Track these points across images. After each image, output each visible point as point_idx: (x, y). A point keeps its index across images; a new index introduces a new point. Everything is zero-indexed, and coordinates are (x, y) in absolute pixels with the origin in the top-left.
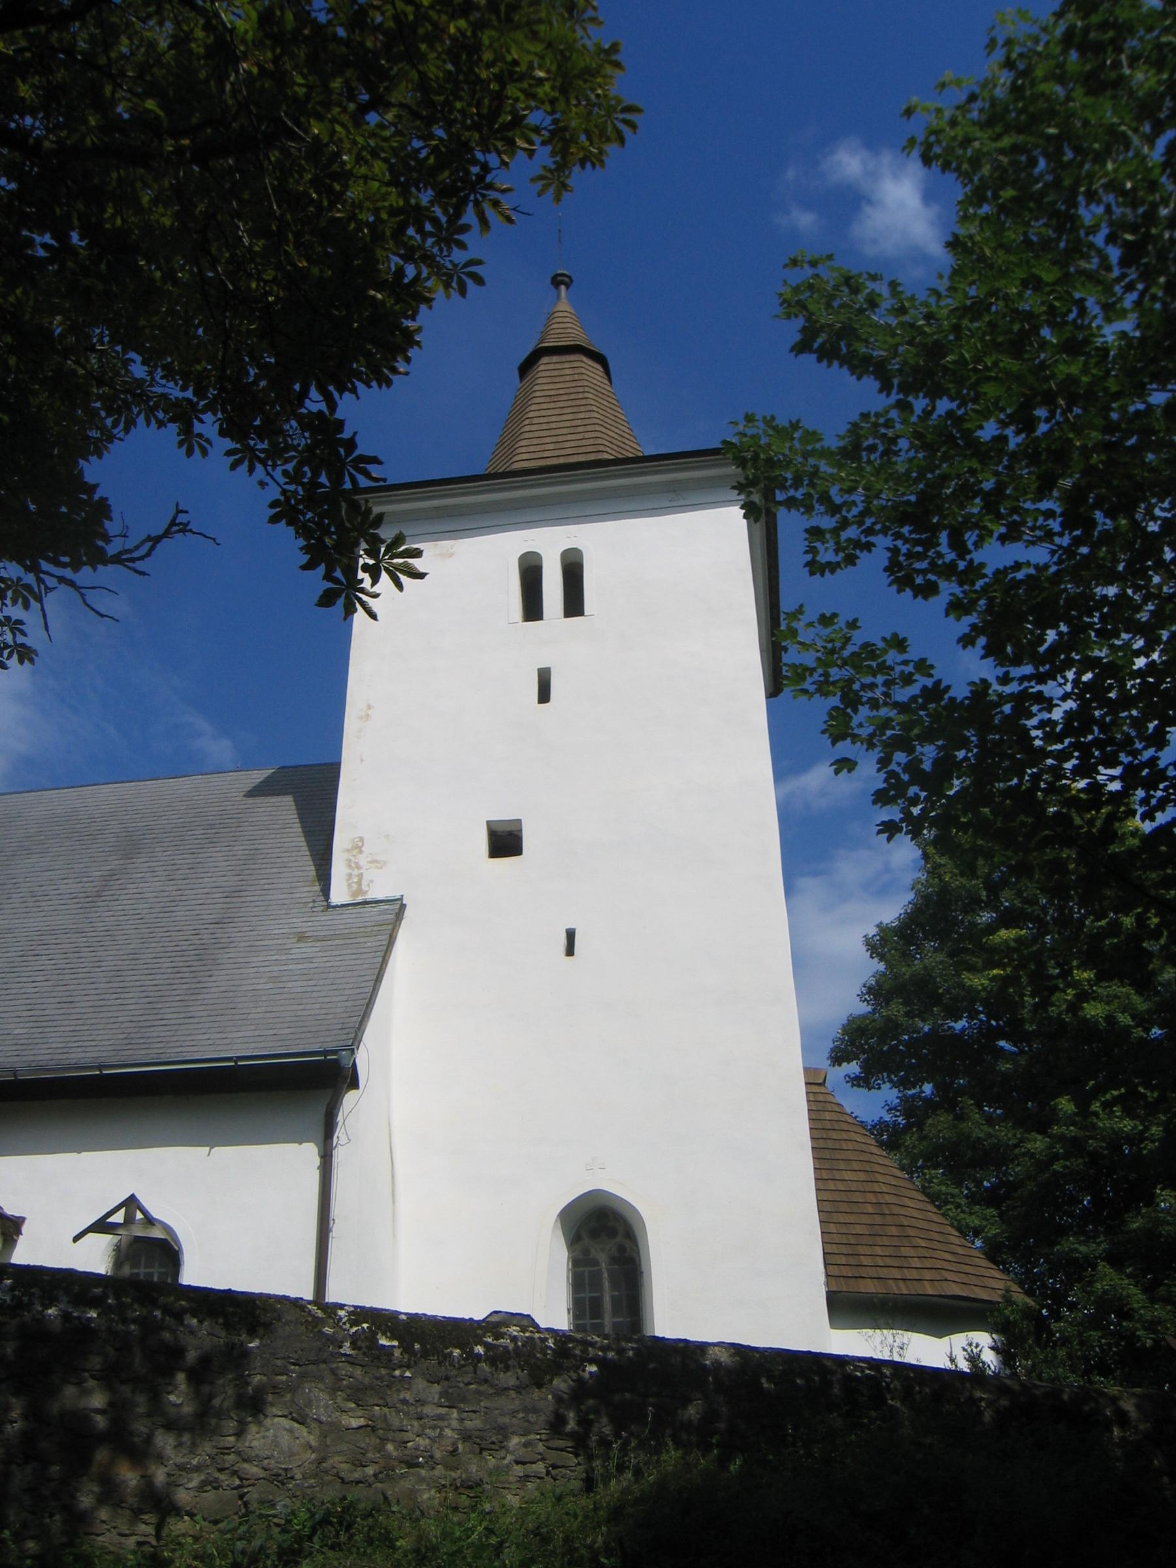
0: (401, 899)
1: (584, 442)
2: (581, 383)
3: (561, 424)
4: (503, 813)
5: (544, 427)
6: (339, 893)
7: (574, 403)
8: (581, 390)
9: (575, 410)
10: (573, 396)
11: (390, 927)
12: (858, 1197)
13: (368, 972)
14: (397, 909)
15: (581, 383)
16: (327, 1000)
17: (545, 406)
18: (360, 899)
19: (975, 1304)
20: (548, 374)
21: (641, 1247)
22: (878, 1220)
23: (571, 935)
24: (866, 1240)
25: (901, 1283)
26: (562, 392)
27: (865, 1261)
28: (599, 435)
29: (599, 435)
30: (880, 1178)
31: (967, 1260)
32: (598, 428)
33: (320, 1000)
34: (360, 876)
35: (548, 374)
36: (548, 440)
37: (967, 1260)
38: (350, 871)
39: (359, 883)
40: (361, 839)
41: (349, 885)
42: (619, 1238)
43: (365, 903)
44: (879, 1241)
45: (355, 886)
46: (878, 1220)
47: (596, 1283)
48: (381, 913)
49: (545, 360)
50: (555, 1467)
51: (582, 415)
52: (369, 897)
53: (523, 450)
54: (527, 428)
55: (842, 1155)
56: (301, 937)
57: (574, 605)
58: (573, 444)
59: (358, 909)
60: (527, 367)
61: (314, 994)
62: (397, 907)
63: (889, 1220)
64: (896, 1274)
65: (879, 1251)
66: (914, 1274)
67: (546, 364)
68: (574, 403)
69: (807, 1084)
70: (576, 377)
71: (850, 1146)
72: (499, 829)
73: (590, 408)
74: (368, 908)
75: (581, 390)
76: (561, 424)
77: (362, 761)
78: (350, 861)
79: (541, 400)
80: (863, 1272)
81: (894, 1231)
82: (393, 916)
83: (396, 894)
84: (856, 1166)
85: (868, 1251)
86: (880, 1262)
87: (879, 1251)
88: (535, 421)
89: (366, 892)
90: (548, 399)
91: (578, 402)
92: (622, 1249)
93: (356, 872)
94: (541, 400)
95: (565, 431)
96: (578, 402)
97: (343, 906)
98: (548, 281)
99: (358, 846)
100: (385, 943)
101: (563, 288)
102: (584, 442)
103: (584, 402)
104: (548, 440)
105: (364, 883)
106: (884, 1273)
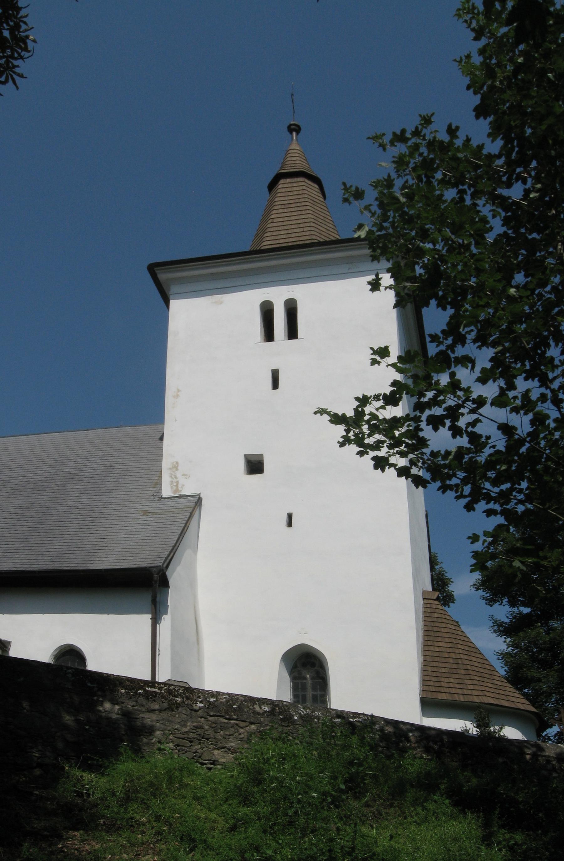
0: (199, 495)
1: (304, 234)
2: (303, 196)
3: (291, 223)
4: (253, 451)
5: (280, 224)
6: (166, 492)
7: (298, 209)
8: (303, 200)
9: (299, 213)
10: (298, 204)
11: (192, 509)
12: (446, 655)
13: (177, 531)
14: (198, 501)
15: (303, 196)
16: (153, 543)
17: (281, 211)
18: (177, 494)
19: (501, 708)
20: (284, 190)
21: (326, 670)
22: (455, 666)
23: (290, 516)
24: (446, 675)
25: (461, 696)
26: (291, 202)
27: (443, 684)
28: (313, 229)
29: (313, 229)
30: (460, 646)
31: (501, 688)
32: (312, 224)
33: (150, 544)
34: (177, 482)
35: (284, 190)
36: (282, 232)
37: (501, 688)
38: (171, 479)
39: (177, 486)
40: (177, 463)
41: (172, 487)
42: (316, 668)
43: (180, 497)
44: (453, 676)
45: (175, 488)
46: (455, 666)
47: (304, 688)
48: (188, 502)
49: (282, 181)
50: (178, 745)
51: (303, 217)
52: (183, 493)
53: (268, 239)
54: (270, 225)
55: (441, 635)
56: (145, 513)
57: (292, 333)
58: (297, 235)
59: (176, 499)
60: (272, 185)
61: (148, 541)
62: (197, 499)
63: (461, 666)
64: (459, 691)
65: (452, 680)
66: (469, 692)
67: (283, 183)
68: (298, 209)
69: (424, 599)
70: (300, 192)
71: (446, 630)
72: (252, 459)
73: (308, 212)
74: (182, 500)
75: (303, 200)
76: (291, 223)
77: (176, 420)
78: (172, 474)
79: (279, 207)
80: (442, 689)
81: (463, 672)
82: (194, 504)
83: (197, 492)
84: (447, 640)
85: (446, 680)
86: (451, 685)
87: (452, 680)
88: (275, 220)
89: (181, 491)
90: (283, 207)
91: (301, 208)
92: (318, 673)
93: (175, 480)
94: (279, 207)
95: (293, 227)
96: (301, 208)
97: (169, 498)
98: (286, 130)
99: (175, 467)
100: (187, 517)
101: (294, 134)
102: (304, 234)
103: (305, 208)
104: (282, 232)
105: (180, 486)
106: (453, 691)
